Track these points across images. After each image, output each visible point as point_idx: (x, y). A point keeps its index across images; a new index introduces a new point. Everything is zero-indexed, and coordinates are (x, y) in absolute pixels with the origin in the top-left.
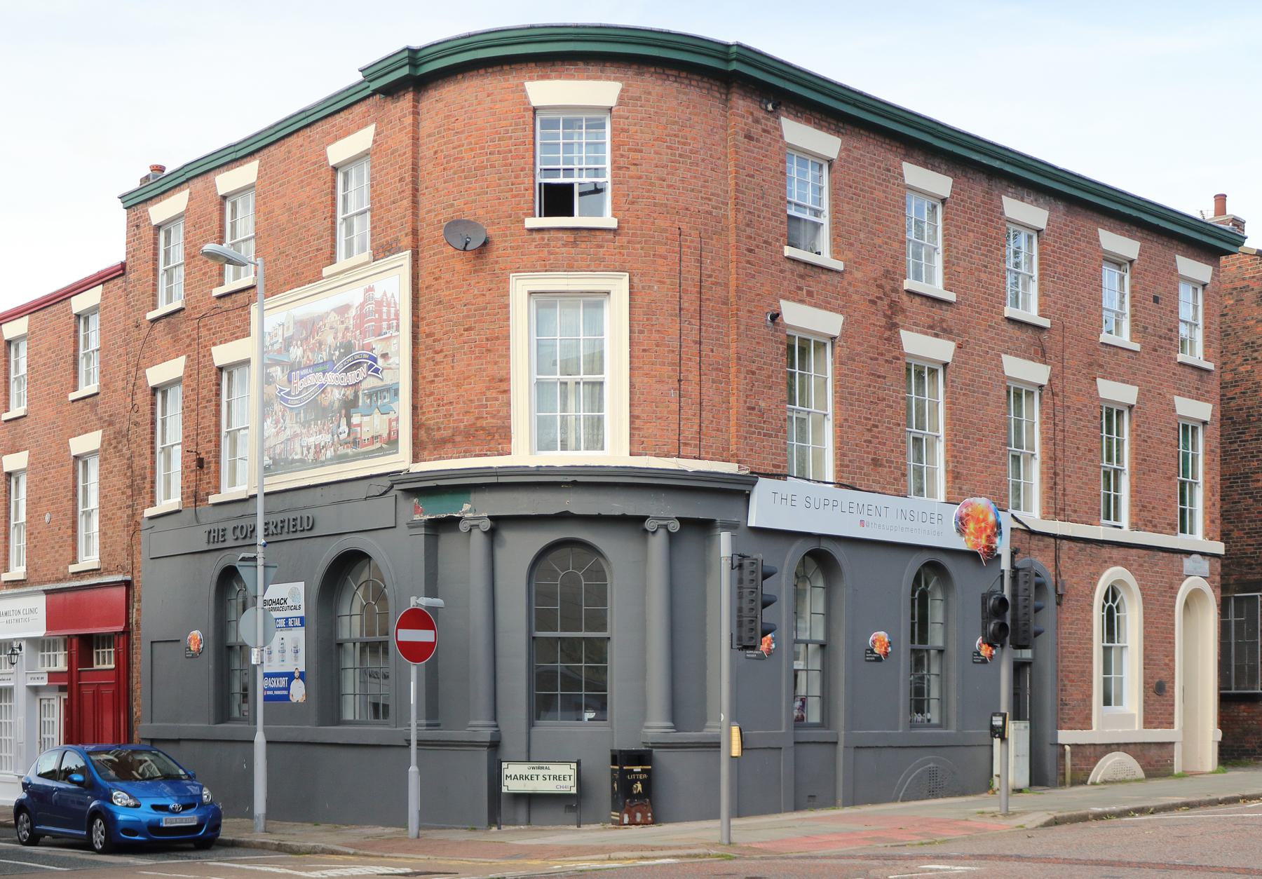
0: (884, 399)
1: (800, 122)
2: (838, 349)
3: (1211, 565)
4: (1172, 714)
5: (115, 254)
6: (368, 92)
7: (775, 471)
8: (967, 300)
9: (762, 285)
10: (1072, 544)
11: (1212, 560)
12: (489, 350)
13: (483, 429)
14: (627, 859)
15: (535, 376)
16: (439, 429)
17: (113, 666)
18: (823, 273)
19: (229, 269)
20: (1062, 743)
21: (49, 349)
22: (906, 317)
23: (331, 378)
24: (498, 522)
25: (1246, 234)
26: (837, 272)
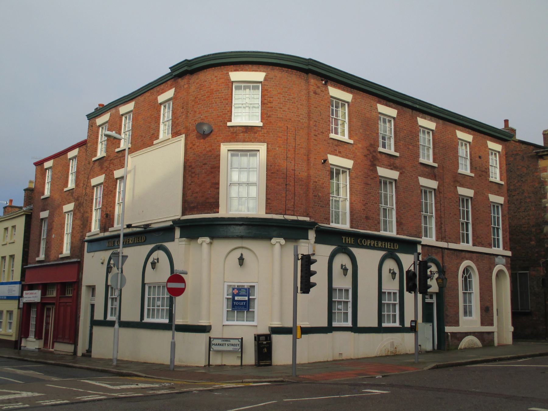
0: (370, 193)
1: (336, 88)
3: (506, 260)
4: (492, 320)
5: (84, 136)
8: (404, 156)
9: (320, 148)
10: (449, 251)
11: (507, 258)
18: (345, 145)
20: (447, 332)
21: (59, 172)
22: (379, 162)
26: (351, 144)
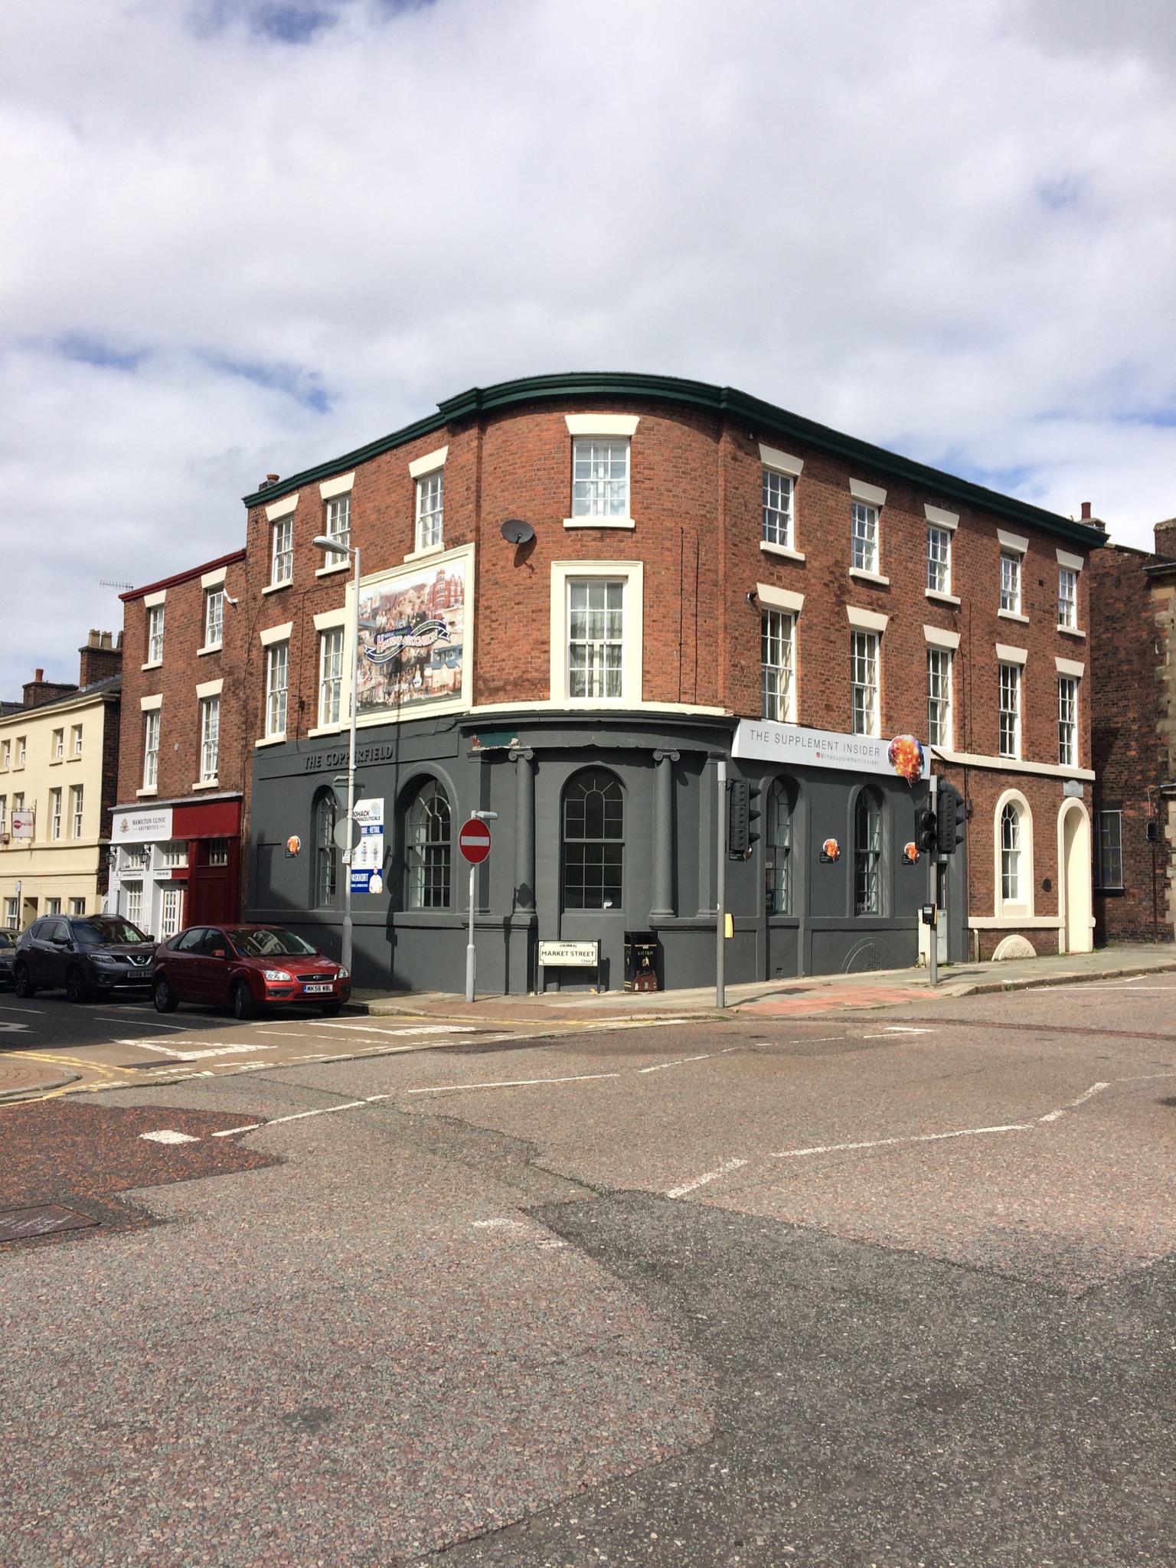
2: (799, 621)
4: (1056, 905)
5: (238, 544)
6: (443, 421)
7: (752, 714)
12: (534, 620)
13: (528, 680)
14: (644, 1020)
15: (570, 640)
16: (494, 680)
17: (225, 864)
19: (329, 555)
23: (408, 640)
24: (542, 755)
25: (1107, 532)
